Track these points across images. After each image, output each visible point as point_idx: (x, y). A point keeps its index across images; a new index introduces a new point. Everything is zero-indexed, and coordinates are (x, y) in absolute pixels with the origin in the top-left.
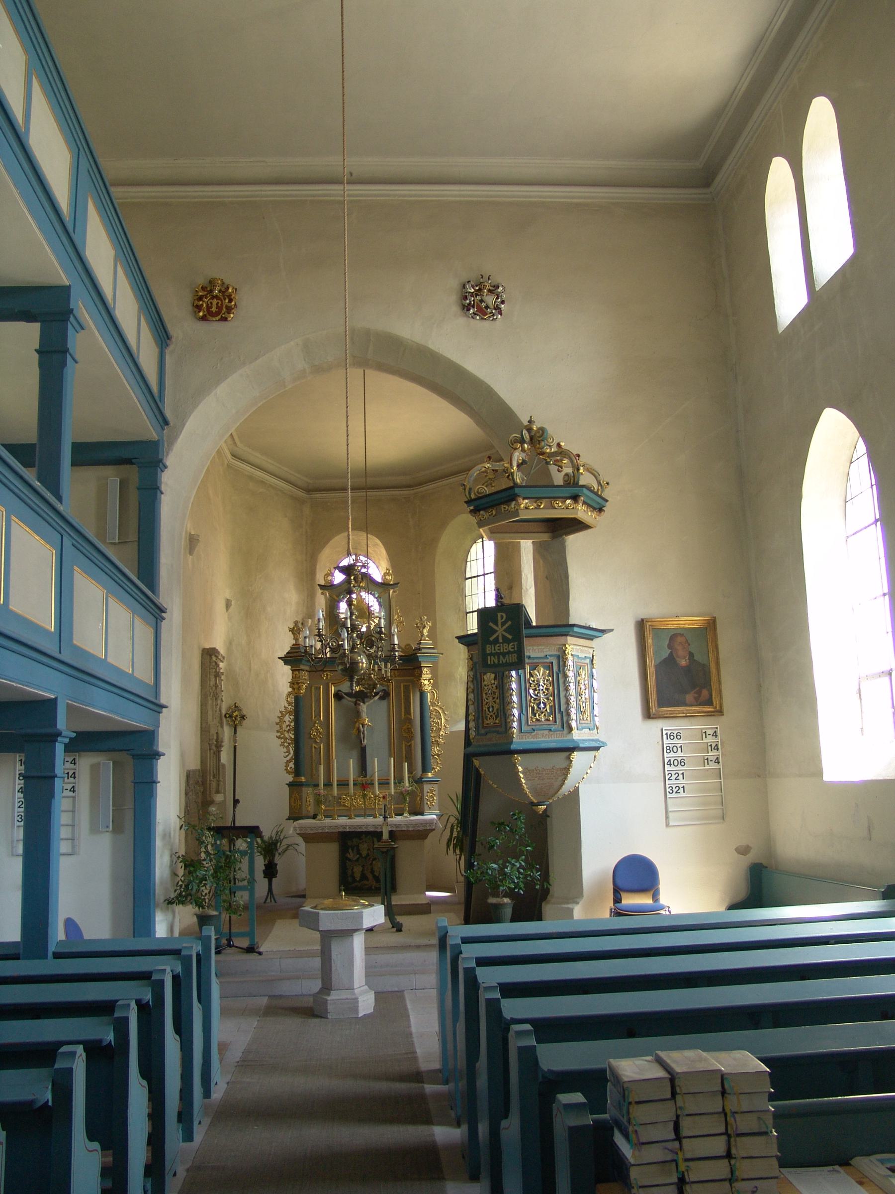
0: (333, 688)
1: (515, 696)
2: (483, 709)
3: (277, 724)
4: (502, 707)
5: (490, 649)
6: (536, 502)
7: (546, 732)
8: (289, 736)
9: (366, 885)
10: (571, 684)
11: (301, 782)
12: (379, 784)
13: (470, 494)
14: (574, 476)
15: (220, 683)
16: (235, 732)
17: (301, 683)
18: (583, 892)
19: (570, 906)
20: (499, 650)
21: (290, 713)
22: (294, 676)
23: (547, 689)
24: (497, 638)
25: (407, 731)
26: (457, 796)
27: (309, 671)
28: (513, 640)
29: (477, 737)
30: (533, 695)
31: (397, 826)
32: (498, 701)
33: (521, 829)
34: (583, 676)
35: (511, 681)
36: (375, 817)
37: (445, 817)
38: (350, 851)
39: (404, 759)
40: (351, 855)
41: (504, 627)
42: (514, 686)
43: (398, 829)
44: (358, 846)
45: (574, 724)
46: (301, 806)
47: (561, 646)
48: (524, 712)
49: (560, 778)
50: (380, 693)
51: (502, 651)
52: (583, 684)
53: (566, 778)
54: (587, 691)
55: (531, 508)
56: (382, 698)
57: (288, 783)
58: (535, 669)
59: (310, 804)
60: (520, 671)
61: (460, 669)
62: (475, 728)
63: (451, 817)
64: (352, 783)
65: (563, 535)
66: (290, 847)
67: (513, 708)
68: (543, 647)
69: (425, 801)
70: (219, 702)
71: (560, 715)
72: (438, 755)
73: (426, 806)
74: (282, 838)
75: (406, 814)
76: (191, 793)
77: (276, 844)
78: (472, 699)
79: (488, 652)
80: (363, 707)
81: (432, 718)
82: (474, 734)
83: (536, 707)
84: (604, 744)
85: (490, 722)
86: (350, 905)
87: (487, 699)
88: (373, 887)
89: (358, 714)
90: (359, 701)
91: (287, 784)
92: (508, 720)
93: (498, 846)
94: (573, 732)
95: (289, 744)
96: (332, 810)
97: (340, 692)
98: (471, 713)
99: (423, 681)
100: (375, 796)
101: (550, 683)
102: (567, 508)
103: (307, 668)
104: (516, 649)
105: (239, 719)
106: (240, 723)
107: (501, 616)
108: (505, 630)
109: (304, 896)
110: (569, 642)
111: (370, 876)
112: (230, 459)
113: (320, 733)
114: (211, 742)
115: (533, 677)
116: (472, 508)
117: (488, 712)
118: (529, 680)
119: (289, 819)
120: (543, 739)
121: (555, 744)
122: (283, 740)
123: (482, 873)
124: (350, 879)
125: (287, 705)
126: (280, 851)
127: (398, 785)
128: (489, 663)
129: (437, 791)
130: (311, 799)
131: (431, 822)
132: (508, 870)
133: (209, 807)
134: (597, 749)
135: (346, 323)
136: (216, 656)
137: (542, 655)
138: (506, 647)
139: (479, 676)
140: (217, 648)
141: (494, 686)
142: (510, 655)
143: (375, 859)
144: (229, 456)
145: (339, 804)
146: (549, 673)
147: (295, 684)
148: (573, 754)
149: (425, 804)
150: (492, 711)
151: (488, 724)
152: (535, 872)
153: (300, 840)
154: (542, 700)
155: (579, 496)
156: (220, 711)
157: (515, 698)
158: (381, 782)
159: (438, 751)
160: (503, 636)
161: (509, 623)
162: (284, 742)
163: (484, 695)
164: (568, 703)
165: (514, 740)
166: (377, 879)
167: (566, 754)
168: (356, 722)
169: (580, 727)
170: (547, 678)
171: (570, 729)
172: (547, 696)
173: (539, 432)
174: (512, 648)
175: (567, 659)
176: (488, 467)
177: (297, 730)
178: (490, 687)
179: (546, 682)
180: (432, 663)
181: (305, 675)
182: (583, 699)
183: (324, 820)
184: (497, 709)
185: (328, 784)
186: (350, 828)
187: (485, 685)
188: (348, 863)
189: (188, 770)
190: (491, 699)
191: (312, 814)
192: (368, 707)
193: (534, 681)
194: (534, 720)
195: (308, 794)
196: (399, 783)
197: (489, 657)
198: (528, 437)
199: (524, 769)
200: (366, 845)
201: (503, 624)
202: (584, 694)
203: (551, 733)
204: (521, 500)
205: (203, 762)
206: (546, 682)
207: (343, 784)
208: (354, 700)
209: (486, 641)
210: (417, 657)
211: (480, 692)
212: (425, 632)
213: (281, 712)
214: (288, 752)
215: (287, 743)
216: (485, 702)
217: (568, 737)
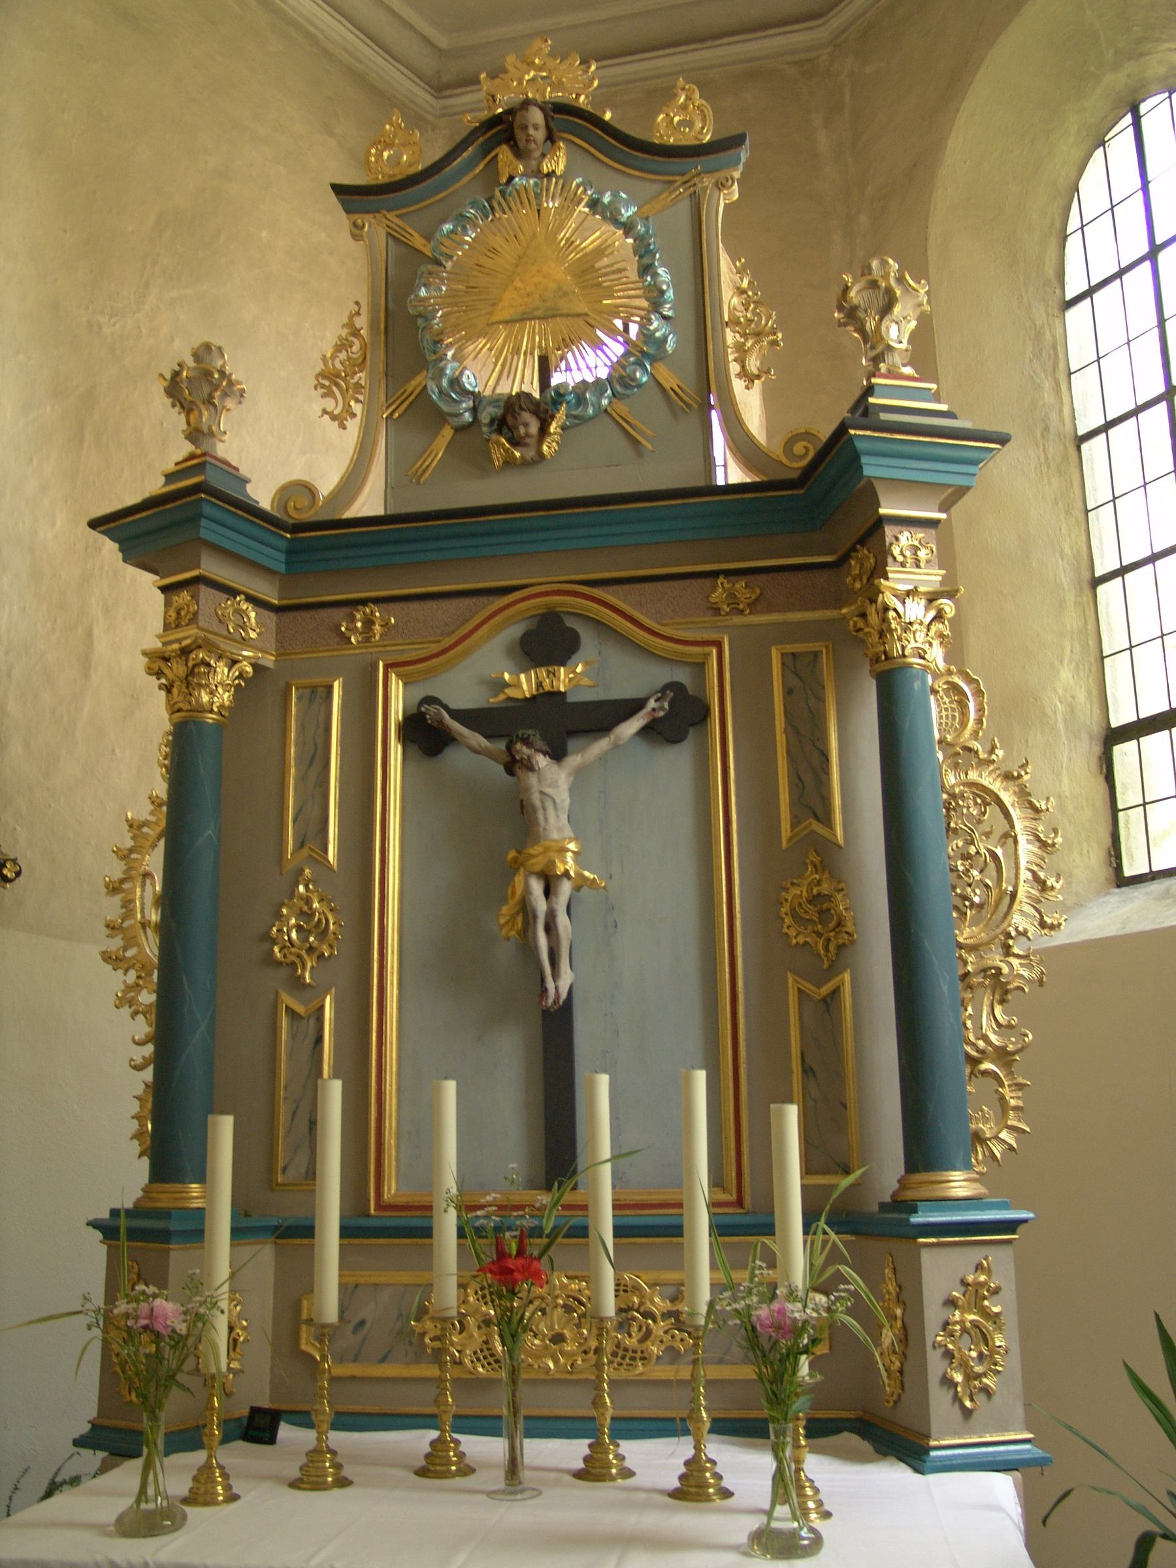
0: (397, 689)
25: (812, 913)
50: (652, 703)
61: (1066, 674)
69: (935, 1365)
73: (939, 1400)
90: (526, 742)
91: (95, 1224)
103: (269, 592)
129: (1009, 1292)
158: (633, 1218)
168: (516, 866)
192: (579, 774)
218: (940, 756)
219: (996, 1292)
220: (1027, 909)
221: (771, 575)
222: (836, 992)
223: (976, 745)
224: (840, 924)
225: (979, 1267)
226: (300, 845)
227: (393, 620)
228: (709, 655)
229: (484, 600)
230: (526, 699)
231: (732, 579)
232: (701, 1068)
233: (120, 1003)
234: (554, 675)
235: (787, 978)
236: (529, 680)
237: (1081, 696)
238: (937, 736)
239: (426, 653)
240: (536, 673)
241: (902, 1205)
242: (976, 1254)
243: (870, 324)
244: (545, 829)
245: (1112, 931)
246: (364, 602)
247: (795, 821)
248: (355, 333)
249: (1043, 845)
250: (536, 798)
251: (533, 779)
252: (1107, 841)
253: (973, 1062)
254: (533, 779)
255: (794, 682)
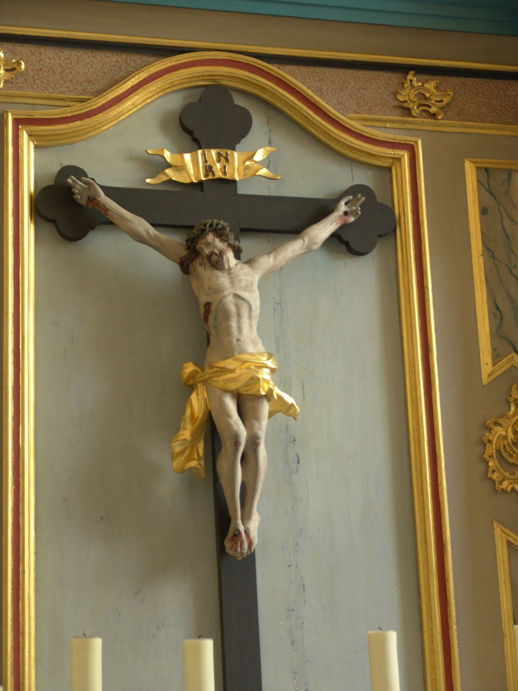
50: (342, 207)
221: (461, 79)
227: (23, 66)
229: (135, 59)
230: (192, 184)
231: (424, 77)
232: (393, 629)
234: (227, 160)
235: (493, 529)
236: (195, 162)
239: (68, 112)
240: (204, 155)
244: (238, 340)
247: (496, 357)
250: (230, 302)
251: (223, 279)
255: (489, 201)
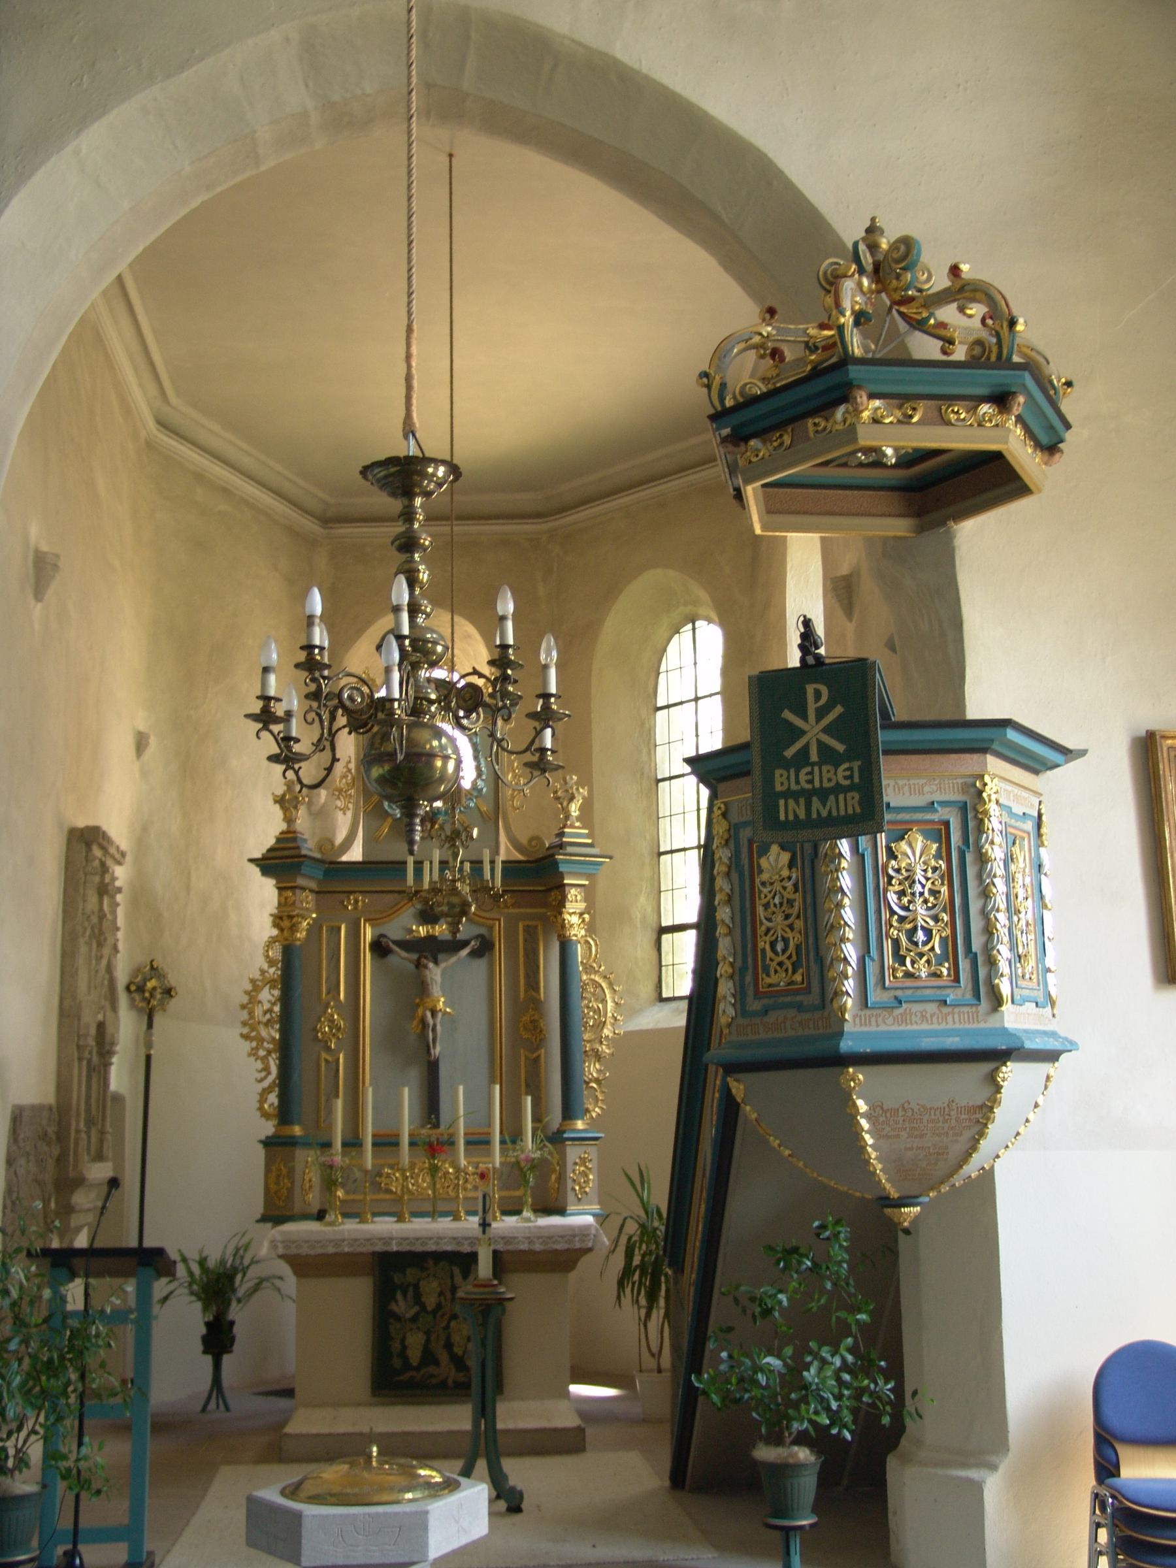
1: (848, 909)
2: (755, 945)
3: (243, 1007)
4: (811, 940)
5: (784, 779)
6: (900, 407)
7: (932, 1008)
8: (269, 1034)
9: (432, 1376)
10: (998, 881)
11: (293, 1137)
12: (468, 1143)
13: (722, 399)
14: (999, 344)
15: (114, 913)
16: (150, 1025)
17: (298, 915)
18: (1006, 1439)
19: (973, 1474)
20: (811, 782)
21: (272, 983)
22: (283, 900)
23: (935, 893)
24: (805, 749)
26: (640, 1169)
27: (318, 893)
28: (848, 757)
29: (740, 1021)
30: (896, 908)
31: (507, 1240)
32: (799, 924)
33: (839, 1263)
34: (1021, 865)
35: (838, 869)
36: (457, 1218)
37: (616, 1221)
38: (399, 1296)
39: (523, 1088)
40: (401, 1306)
41: (825, 721)
42: (846, 881)
43: (510, 1248)
44: (417, 1287)
45: (1005, 988)
46: (291, 1191)
47: (970, 780)
48: (874, 952)
49: (967, 1134)
50: (473, 943)
51: (817, 784)
52: (1021, 883)
53: (982, 1134)
54: (1029, 902)
55: (887, 421)
56: (476, 954)
57: (263, 1138)
58: (902, 838)
59: (311, 1187)
60: (863, 841)
61: (643, 899)
62: (734, 996)
63: (629, 1221)
64: (405, 1140)
65: (948, 518)
66: (265, 1284)
67: (843, 940)
68: (922, 782)
69: (570, 1184)
70: (106, 951)
71: (968, 961)
72: (597, 1081)
73: (571, 1197)
74: (246, 1262)
75: (527, 1214)
76: (22, 1161)
77: (231, 1278)
78: (728, 921)
79: (778, 788)
80: (435, 973)
81: (585, 998)
82: (731, 1011)
83: (903, 939)
84: (1071, 1046)
85: (779, 979)
86: (391, 1489)
87: (769, 920)
88: (450, 1382)
89: (423, 988)
90: (426, 958)
92: (832, 974)
93: (782, 1310)
94: (1003, 1008)
95: (269, 1052)
96: (360, 1201)
97: (384, 940)
98: (724, 958)
99: (566, 917)
100: (458, 1170)
101: (942, 877)
102: (980, 425)
103: (313, 885)
104: (856, 780)
105: (159, 996)
106: (162, 1003)
107: (815, 693)
108: (825, 730)
109: (289, 1393)
110: (989, 768)
111: (444, 1357)
112: (155, 432)
113: (339, 1029)
114: (81, 1043)
115: (895, 858)
116: (726, 431)
117: (769, 954)
118: (885, 867)
119: (264, 1219)
120: (924, 1027)
121: (957, 1039)
122: (254, 1044)
123: (741, 1380)
124: (397, 1363)
125: (265, 966)
126: (241, 1292)
127: (510, 1145)
128: (782, 817)
129: (595, 1161)
130: (314, 1176)
131: (583, 1231)
132: (810, 1375)
133: (72, 1192)
134: (1051, 1056)
135: (410, 158)
136: (104, 849)
137: (920, 801)
138: (830, 775)
139: (745, 862)
140: (105, 828)
141: (789, 885)
142: (841, 797)
143: (454, 1317)
144: (151, 424)
145: (377, 1187)
146: (939, 849)
147: (284, 918)
148: (1004, 1069)
149: (569, 1189)
150: (784, 951)
151: (770, 985)
152: (881, 1382)
153: (285, 1269)
154: (920, 922)
155: (1014, 393)
156: (110, 969)
157: (849, 915)
159: (599, 1071)
160: (823, 747)
161: (839, 710)
162: (257, 1048)
163: (760, 910)
164: (989, 930)
165: (847, 1028)
166: (459, 1363)
167: (985, 1067)
168: (418, 1005)
169: (1017, 997)
170: (933, 863)
171: (997, 1000)
172: (932, 912)
173: (898, 249)
174: (845, 778)
175: (986, 813)
176: (769, 334)
177: (286, 1020)
178: (777, 887)
179: (929, 874)
180: (589, 876)
181: (307, 900)
182: (1023, 922)
183: (343, 1223)
184: (798, 947)
185: (353, 1143)
186: (399, 1244)
187: (763, 884)
188: (395, 1327)
189: (13, 1106)
190: (779, 918)
191: (315, 1209)
193: (898, 871)
194: (899, 974)
195: (307, 1162)
196: (514, 1142)
197: (782, 802)
198: (870, 260)
199: (872, 1107)
200: (435, 1284)
201: (821, 713)
202: (1024, 913)
203: (945, 1010)
204: (865, 398)
205: (62, 1086)
206: (929, 874)
207: (386, 1143)
208: (415, 956)
209: (774, 759)
210: (556, 864)
211: (748, 904)
212: (574, 809)
213: (253, 981)
214: (267, 1069)
215: (264, 1049)
216: (763, 928)
217: (992, 1022)
218: (581, 969)
219: (590, 1160)
220: (609, 1027)
222: (538, 1057)
223: (595, 965)
224: (541, 1031)
225: (585, 1153)
226: (328, 993)
228: (494, 924)
233: (250, 1055)
237: (649, 910)
238: (580, 960)
241: (560, 1132)
242: (584, 1148)
243: (565, 804)
245: (650, 1027)
246: (355, 892)
247: (526, 991)
248: (349, 771)
249: (617, 1004)
250: (429, 981)
252: (657, 980)
253: (587, 1083)
254: (428, 972)
